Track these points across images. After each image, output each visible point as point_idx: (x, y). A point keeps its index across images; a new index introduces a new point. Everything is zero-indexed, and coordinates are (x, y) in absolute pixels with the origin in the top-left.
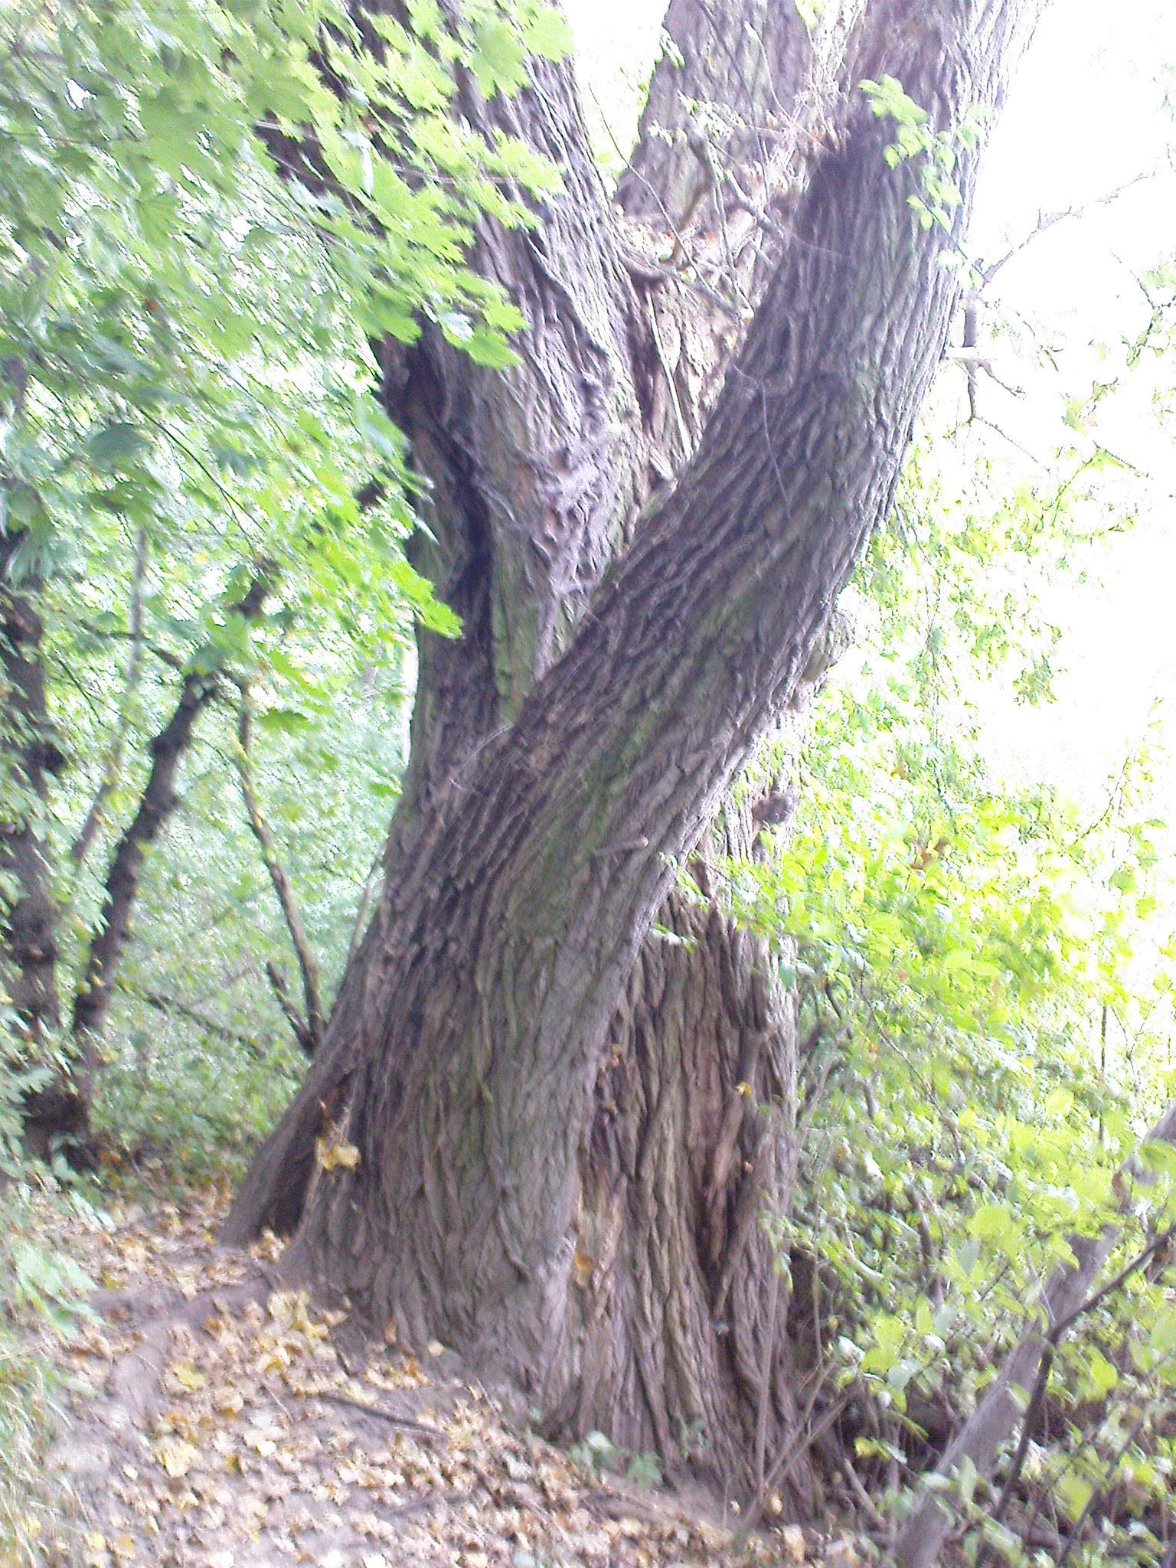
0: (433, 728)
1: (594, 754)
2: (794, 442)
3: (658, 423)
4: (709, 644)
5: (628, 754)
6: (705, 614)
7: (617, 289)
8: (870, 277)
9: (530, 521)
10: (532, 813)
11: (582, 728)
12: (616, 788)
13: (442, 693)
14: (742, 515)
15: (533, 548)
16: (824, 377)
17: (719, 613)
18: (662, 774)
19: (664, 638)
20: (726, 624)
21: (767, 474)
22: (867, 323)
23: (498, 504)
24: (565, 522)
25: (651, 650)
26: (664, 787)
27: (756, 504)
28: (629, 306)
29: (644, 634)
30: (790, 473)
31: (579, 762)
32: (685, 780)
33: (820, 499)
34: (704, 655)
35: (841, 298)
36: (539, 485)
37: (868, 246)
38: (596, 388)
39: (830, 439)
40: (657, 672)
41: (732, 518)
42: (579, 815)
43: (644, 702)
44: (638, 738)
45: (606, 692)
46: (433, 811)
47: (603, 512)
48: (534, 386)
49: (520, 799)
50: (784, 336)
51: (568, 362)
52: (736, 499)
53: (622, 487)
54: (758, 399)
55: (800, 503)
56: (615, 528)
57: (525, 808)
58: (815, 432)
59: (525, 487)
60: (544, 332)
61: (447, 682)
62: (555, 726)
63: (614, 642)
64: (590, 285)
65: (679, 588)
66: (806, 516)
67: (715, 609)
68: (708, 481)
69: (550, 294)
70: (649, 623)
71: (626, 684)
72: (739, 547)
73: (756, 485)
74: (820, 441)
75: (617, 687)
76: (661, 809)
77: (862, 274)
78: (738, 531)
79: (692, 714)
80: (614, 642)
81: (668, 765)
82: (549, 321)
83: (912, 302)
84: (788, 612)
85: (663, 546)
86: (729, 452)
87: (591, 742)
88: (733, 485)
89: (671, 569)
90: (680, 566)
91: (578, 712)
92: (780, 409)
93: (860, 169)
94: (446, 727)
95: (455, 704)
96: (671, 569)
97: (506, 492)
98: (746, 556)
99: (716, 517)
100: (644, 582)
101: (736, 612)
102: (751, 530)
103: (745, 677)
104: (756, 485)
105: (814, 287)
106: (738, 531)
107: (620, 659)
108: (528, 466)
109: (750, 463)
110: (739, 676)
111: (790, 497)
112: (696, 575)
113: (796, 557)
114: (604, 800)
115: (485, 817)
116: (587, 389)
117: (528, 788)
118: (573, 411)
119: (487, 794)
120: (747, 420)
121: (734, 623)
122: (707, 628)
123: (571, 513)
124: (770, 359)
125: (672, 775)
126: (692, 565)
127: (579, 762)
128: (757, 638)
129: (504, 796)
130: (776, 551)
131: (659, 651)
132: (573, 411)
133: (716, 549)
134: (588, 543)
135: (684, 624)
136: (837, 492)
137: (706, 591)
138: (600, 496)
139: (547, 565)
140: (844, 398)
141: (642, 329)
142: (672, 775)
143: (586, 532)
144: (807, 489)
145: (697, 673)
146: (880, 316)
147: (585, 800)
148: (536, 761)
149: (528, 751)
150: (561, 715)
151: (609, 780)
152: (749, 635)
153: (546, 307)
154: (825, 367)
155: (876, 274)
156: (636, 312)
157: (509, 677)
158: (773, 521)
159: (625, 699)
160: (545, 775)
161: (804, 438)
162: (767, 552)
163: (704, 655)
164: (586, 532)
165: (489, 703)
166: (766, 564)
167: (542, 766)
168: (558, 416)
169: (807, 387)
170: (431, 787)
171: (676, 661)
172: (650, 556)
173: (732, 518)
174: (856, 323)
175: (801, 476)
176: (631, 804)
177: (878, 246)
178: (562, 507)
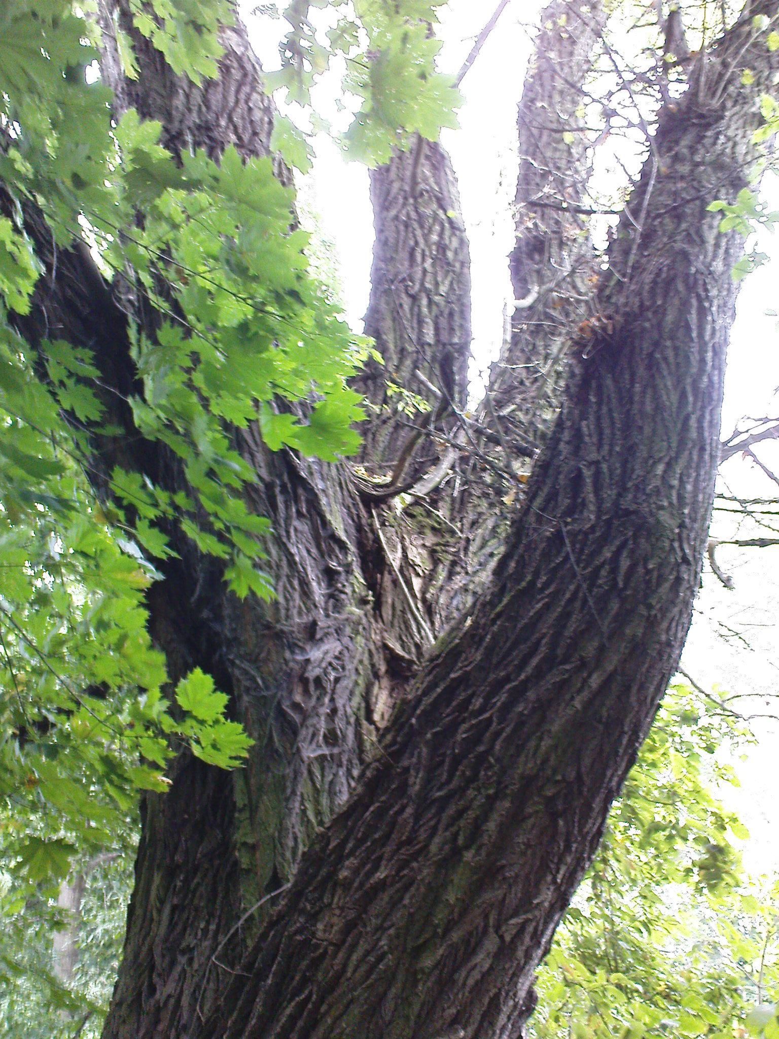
0: (160, 911)
1: (398, 917)
2: (603, 573)
3: (387, 612)
4: (528, 782)
5: (440, 917)
6: (520, 748)
7: (349, 501)
8: (654, 431)
9: (279, 687)
10: (321, 1000)
11: (382, 885)
12: (428, 962)
13: (171, 873)
14: (553, 645)
15: (281, 713)
16: (627, 513)
17: (538, 747)
18: (479, 943)
19: (474, 778)
20: (545, 761)
21: (578, 604)
22: (660, 469)
23: (246, 672)
24: (312, 688)
25: (462, 790)
26: (482, 960)
27: (569, 632)
28: (358, 515)
29: (451, 775)
30: (603, 601)
31: (381, 928)
32: (505, 951)
33: (634, 629)
34: (521, 800)
35: (631, 450)
36: (288, 654)
37: (649, 408)
38: (338, 573)
39: (641, 570)
40: (471, 814)
41: (543, 649)
42: (382, 998)
43: (456, 853)
44: (451, 897)
45: (409, 842)
46: (158, 1009)
47: (346, 683)
48: (284, 563)
49: (305, 981)
50: (577, 481)
51: (314, 551)
52: (545, 628)
53: (361, 662)
54: (558, 537)
55: (616, 633)
56: (357, 700)
57: (312, 991)
58: (625, 563)
59: (274, 657)
60: (296, 523)
61: (178, 858)
62: (347, 885)
63: (416, 783)
64: (331, 492)
65: (489, 721)
66: (623, 647)
67: (532, 744)
68: (510, 615)
69: (300, 491)
70: (457, 761)
71: (434, 831)
72: (553, 678)
73: (566, 616)
74: (632, 569)
75: (423, 835)
76: (478, 988)
77: (647, 430)
78: (550, 661)
79: (515, 866)
80: (416, 783)
81: (485, 932)
82: (300, 514)
83: (695, 457)
84: (607, 749)
85: (464, 680)
86: (532, 583)
87: (394, 903)
88: (540, 615)
89: (477, 703)
90: (487, 699)
91: (376, 868)
92: (584, 543)
93: (632, 352)
94: (174, 909)
95: (187, 882)
96: (477, 703)
97: (254, 660)
98: (562, 686)
99: (524, 648)
100: (447, 714)
101: (555, 747)
102: (565, 661)
103: (566, 822)
104: (566, 616)
105: (600, 440)
106: (550, 661)
107: (424, 803)
108: (279, 635)
109: (555, 596)
110: (561, 823)
111: (605, 625)
112: (506, 708)
113: (615, 689)
114: (413, 979)
115: (258, 1008)
116: (330, 575)
117: (315, 964)
118: (318, 591)
119: (261, 976)
120: (547, 555)
121: (553, 761)
122: (525, 766)
123: (318, 681)
124: (564, 502)
125: (491, 944)
126: (501, 698)
127: (381, 928)
128: (579, 777)
129: (284, 976)
130: (595, 681)
131: (471, 793)
132: (318, 591)
133: (528, 680)
134: (334, 711)
135: (498, 760)
136: (652, 623)
137: (521, 724)
138: (343, 668)
139: (295, 733)
140: (650, 534)
141: (370, 535)
142: (491, 944)
143: (332, 700)
144: (623, 619)
145: (516, 818)
146: (669, 465)
147: (389, 979)
148: (326, 929)
149: (314, 917)
150: (356, 871)
151: (418, 952)
152: (572, 776)
153: (297, 501)
154: (627, 502)
155: (660, 430)
156: (364, 521)
157: (253, 848)
158: (590, 649)
159: (433, 848)
160: (338, 946)
161: (614, 570)
162: (585, 681)
163: (521, 800)
164: (332, 700)
165: (227, 875)
166: (585, 694)
167: (334, 935)
168: (306, 593)
169: (609, 523)
170: (155, 979)
171: (492, 800)
172: (451, 691)
173: (543, 649)
174: (649, 471)
175: (614, 606)
176: (445, 983)
177: (659, 408)
178: (313, 673)
